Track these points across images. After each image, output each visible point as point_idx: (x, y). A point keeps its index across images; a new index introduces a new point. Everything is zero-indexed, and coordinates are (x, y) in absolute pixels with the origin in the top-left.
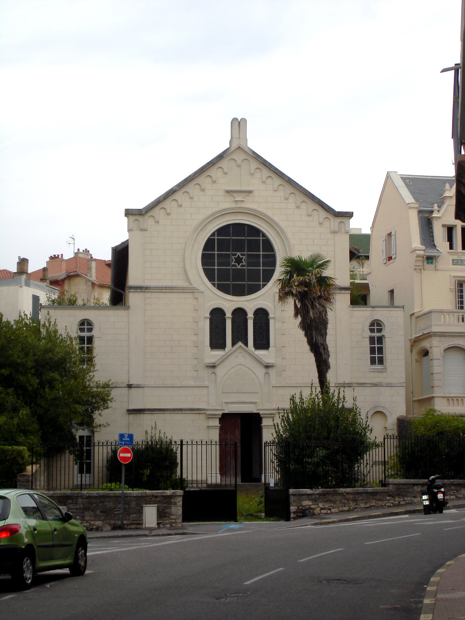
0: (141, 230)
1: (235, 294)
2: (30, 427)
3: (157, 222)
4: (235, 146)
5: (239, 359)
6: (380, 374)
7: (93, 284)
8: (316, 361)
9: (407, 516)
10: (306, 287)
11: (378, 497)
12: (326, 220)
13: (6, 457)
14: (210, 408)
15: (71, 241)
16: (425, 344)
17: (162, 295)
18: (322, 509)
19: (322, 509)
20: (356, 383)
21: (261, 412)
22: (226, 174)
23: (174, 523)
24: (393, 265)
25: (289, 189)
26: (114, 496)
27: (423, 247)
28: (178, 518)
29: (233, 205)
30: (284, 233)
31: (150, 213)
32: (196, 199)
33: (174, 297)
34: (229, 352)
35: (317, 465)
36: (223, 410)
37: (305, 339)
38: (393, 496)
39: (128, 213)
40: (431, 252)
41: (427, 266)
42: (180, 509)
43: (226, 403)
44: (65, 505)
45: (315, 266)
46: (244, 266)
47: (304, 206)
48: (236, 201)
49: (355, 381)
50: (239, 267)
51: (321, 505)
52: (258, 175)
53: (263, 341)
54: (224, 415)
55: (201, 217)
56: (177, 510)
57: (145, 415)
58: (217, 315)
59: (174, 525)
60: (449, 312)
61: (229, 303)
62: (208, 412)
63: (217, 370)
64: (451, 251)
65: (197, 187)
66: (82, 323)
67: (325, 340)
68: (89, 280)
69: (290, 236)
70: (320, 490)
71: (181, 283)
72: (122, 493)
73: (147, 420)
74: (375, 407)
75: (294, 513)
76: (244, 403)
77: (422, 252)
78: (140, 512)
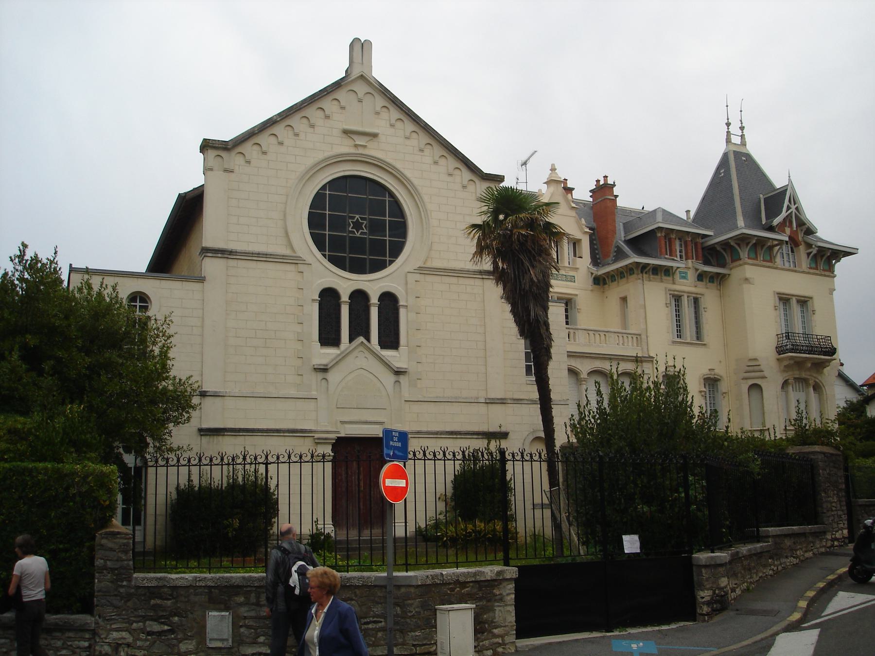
0: (226, 171)
1: (352, 270)
2: (88, 436)
3: (249, 162)
4: (355, 74)
12: (471, 182)
13: (67, 489)
14: (319, 429)
20: (511, 399)
22: (343, 108)
23: (499, 645)
25: (424, 139)
26: (364, 586)
28: (507, 634)
31: (240, 149)
32: (302, 136)
33: (271, 269)
34: (346, 350)
36: (338, 432)
39: (207, 146)
42: (512, 609)
43: (342, 422)
44: (227, 609)
47: (442, 161)
48: (356, 146)
49: (509, 395)
50: (358, 235)
52: (385, 114)
53: (390, 338)
54: (340, 440)
55: (310, 161)
56: (506, 614)
57: (226, 437)
58: (329, 297)
59: (500, 650)
61: (346, 283)
62: (317, 436)
63: (330, 376)
65: (305, 121)
69: (426, 198)
71: (280, 249)
72: (390, 578)
73: (231, 446)
74: (534, 431)
76: (366, 423)
78: (430, 624)
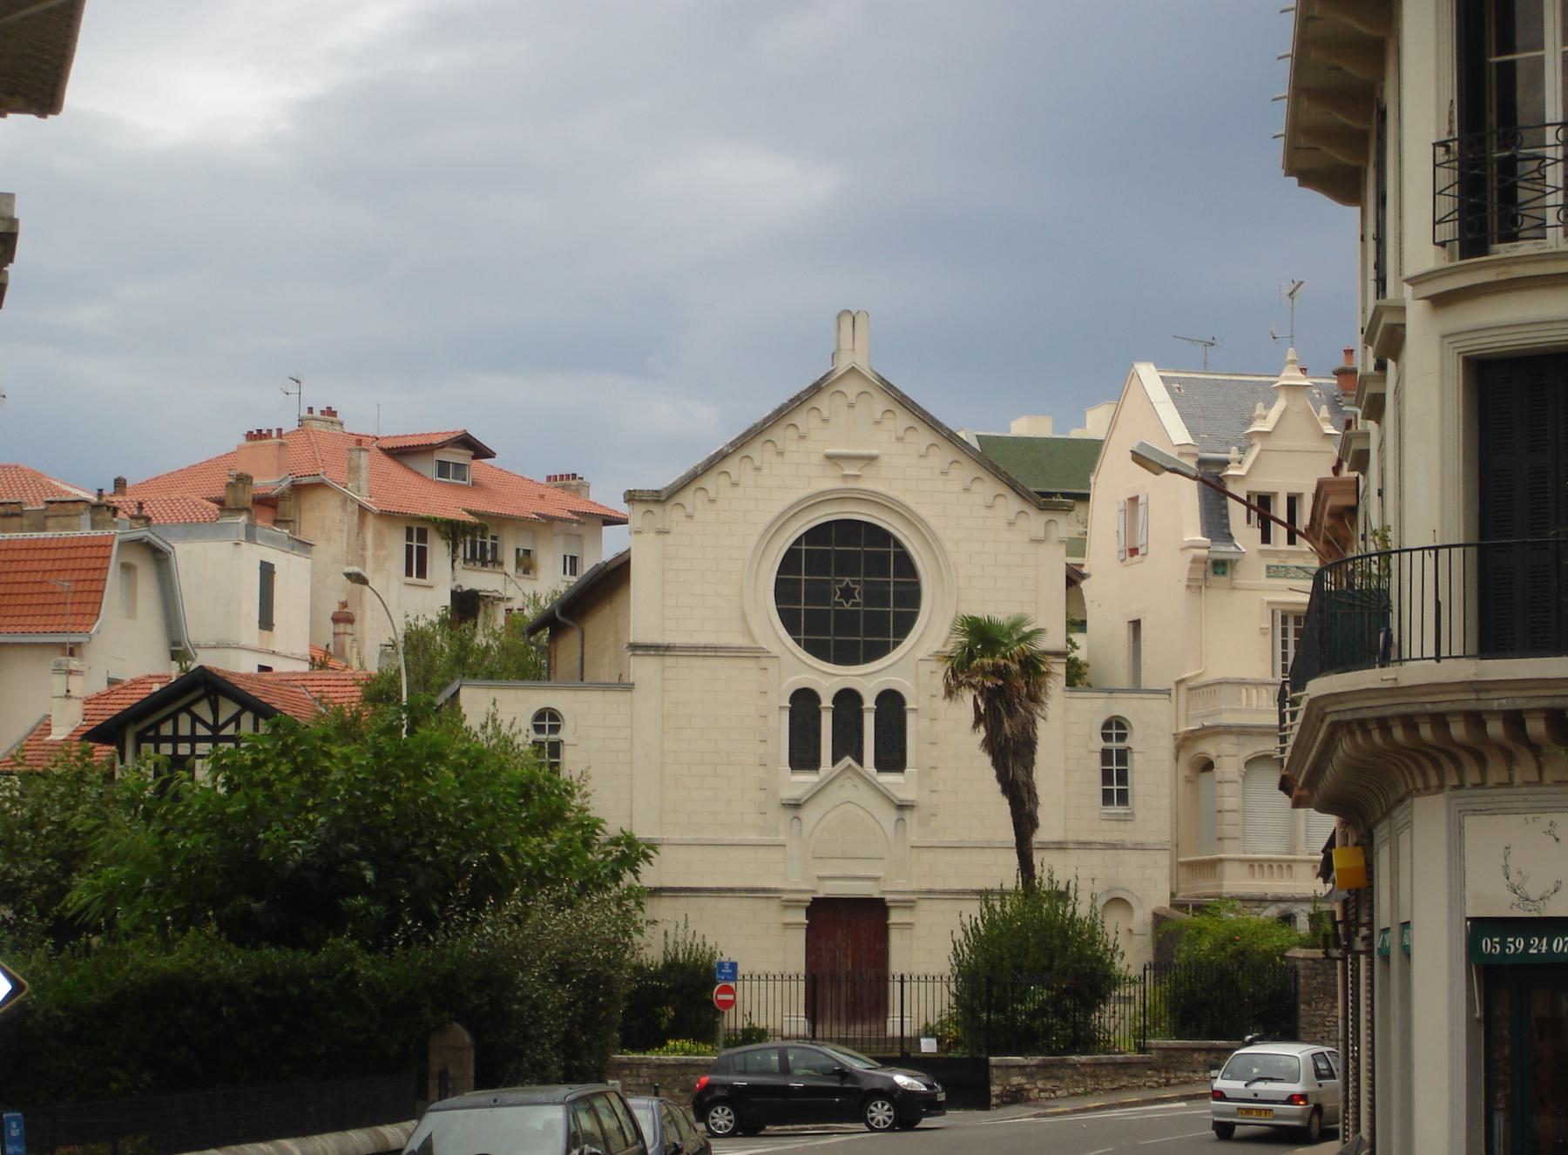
0: (659, 532)
5: (848, 793)
6: (1121, 825)
7: (363, 510)
8: (1013, 814)
9: (1183, 1104)
10: (1001, 678)
11: (1133, 1071)
14: (788, 887)
15: (293, 388)
16: (1209, 748)
17: (698, 662)
18: (1041, 1090)
19: (1041, 1090)
21: (888, 897)
24: (1137, 566)
27: (1207, 541)
29: (839, 485)
30: (937, 540)
31: (677, 499)
32: (765, 470)
35: (1032, 1015)
37: (993, 772)
38: (1157, 1070)
40: (1222, 551)
41: (1214, 579)
45: (1015, 637)
46: (857, 604)
48: (845, 476)
49: (1072, 837)
50: (847, 607)
51: (1040, 1084)
53: (892, 756)
58: (804, 703)
60: (1259, 684)
61: (827, 679)
62: (785, 896)
64: (1266, 547)
66: (540, 715)
67: (1030, 775)
68: (353, 500)
70: (1037, 1059)
74: (1110, 890)
75: (997, 1096)
76: (854, 878)
77: (1205, 552)
